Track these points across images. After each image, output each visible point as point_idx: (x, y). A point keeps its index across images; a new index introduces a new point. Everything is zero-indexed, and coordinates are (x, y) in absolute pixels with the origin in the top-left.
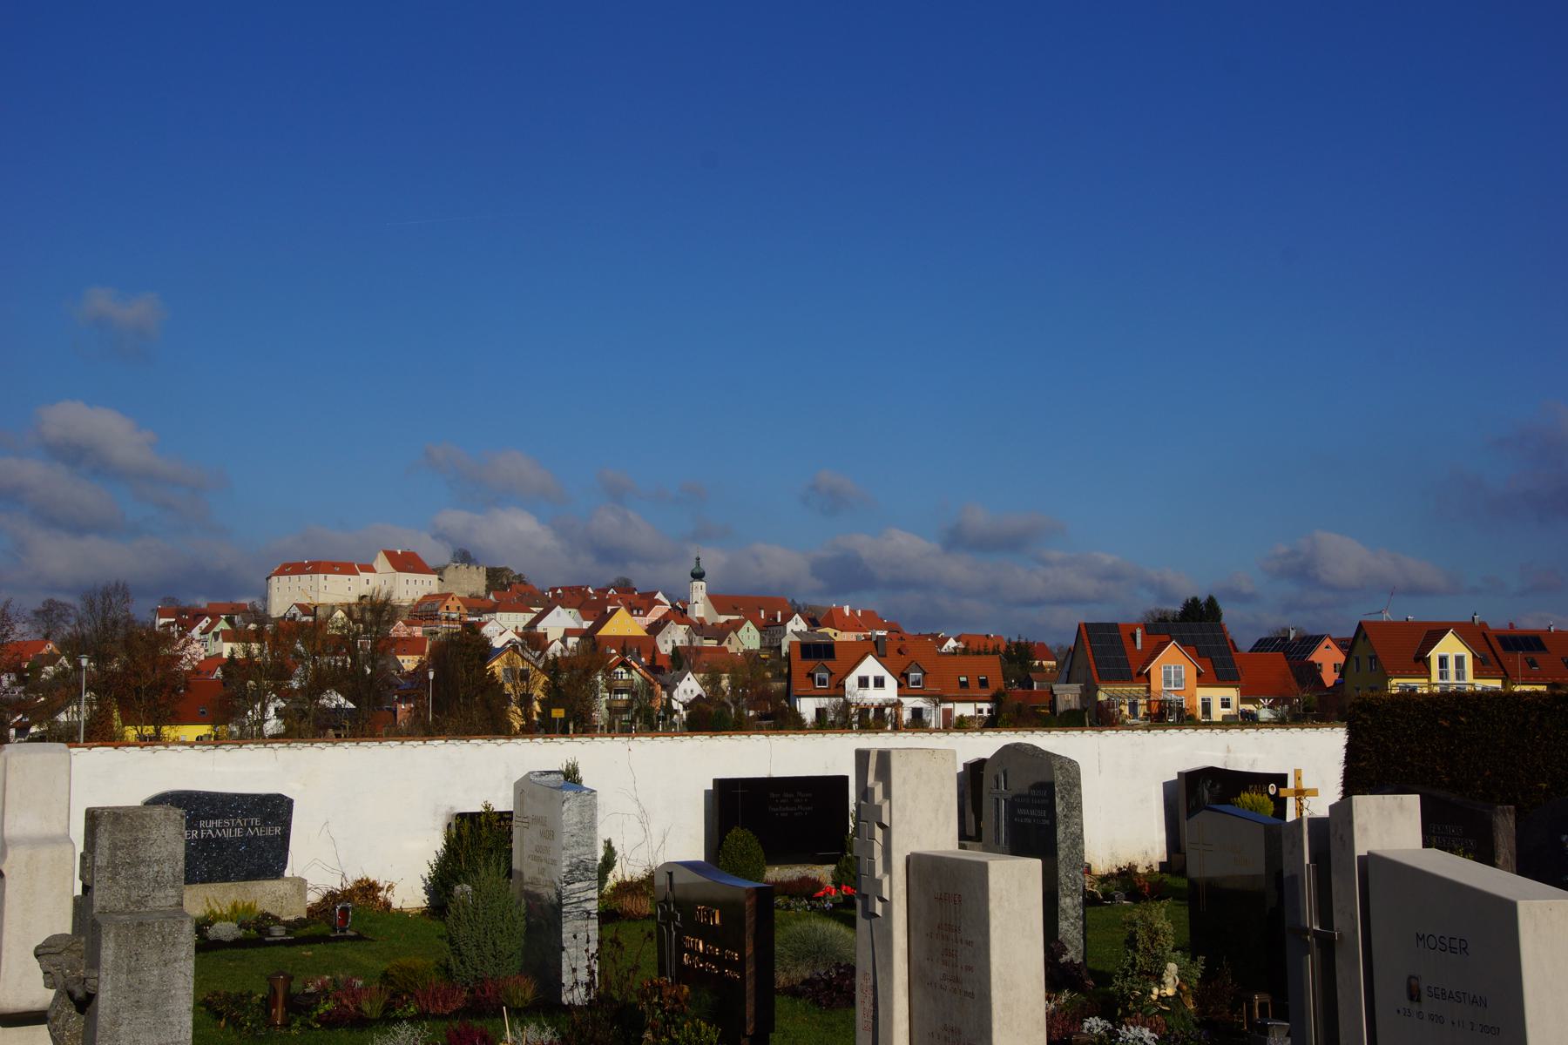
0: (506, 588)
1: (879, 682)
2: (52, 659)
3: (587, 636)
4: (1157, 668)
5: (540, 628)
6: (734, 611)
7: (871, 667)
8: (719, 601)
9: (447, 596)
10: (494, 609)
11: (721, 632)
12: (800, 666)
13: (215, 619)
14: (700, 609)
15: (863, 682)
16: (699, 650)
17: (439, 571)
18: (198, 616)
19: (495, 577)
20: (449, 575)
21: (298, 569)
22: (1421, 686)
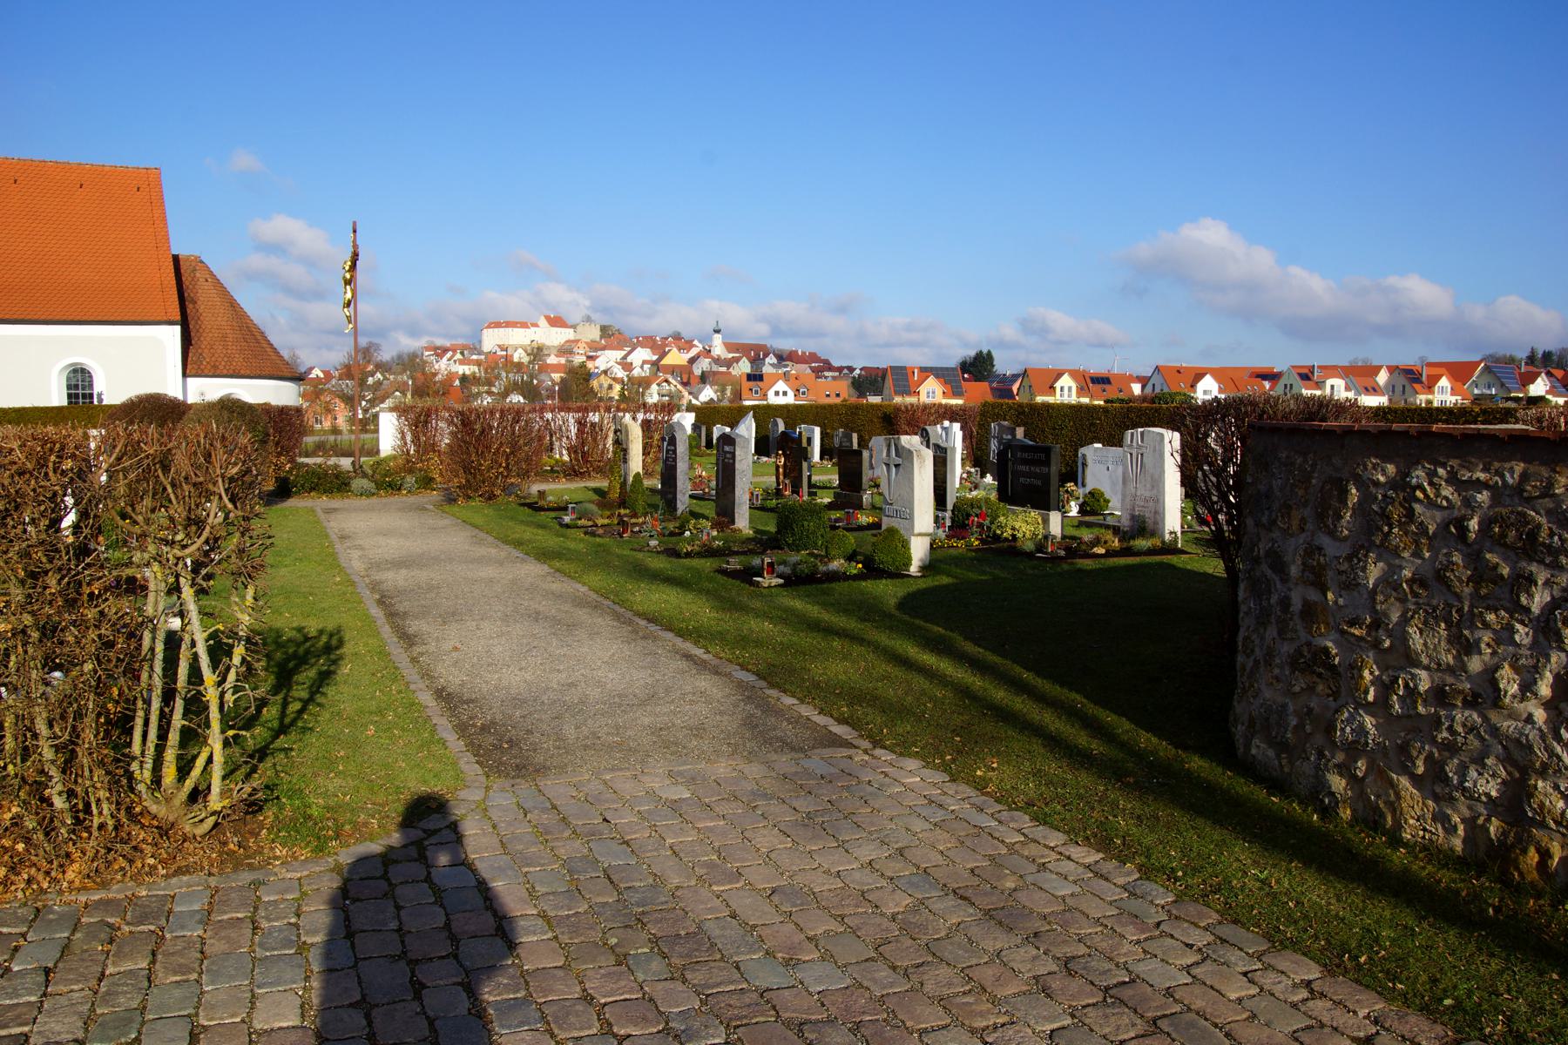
0: (611, 337)
1: (785, 393)
3: (656, 365)
4: (923, 389)
5: (629, 359)
6: (737, 351)
7: (781, 386)
8: (729, 347)
9: (577, 341)
10: (604, 348)
11: (729, 363)
12: (746, 385)
13: (454, 351)
14: (719, 350)
15: (777, 393)
16: (715, 373)
17: (574, 327)
18: (445, 351)
19: (605, 330)
21: (498, 325)
22: (1050, 399)
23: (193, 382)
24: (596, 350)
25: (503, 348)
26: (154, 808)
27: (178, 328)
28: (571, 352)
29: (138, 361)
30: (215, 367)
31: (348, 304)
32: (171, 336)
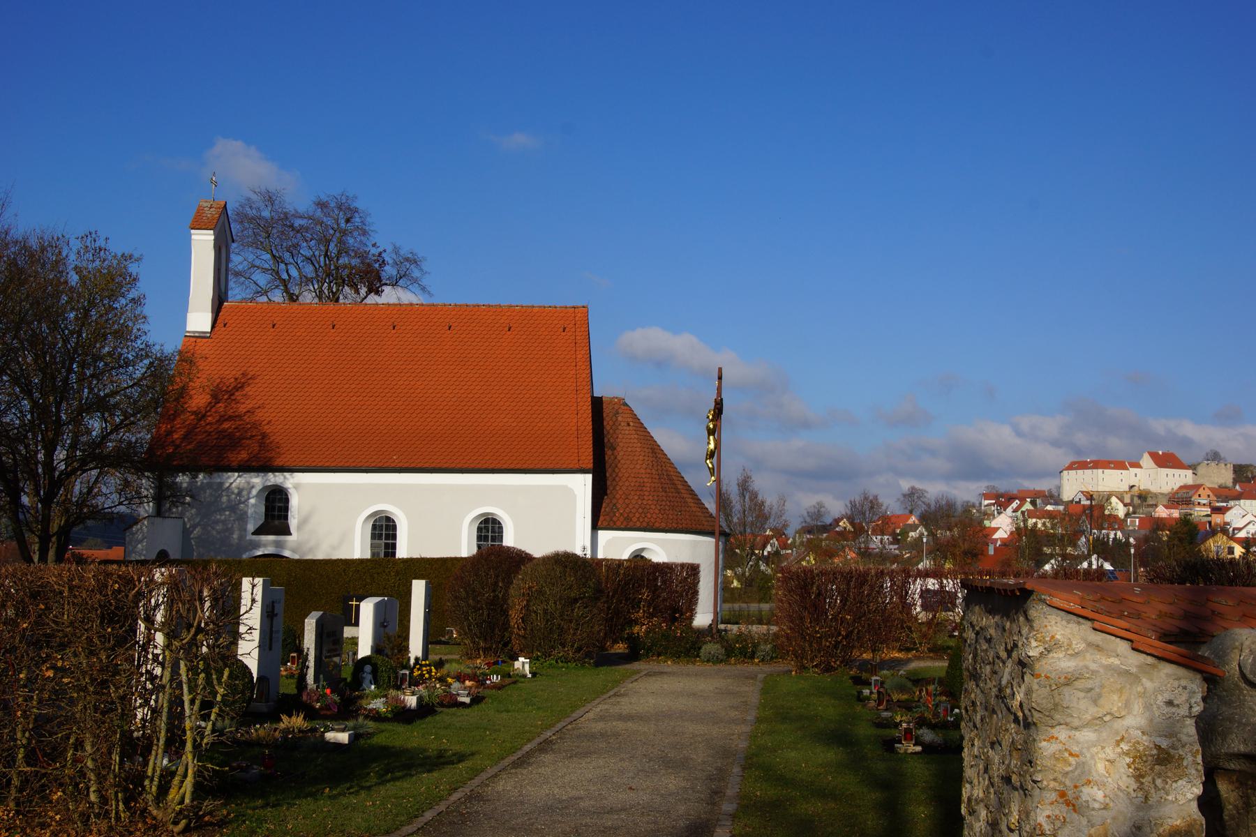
2: (914, 527)
9: (1196, 487)
10: (1239, 497)
13: (1023, 501)
17: (1193, 467)
18: (1011, 499)
19: (1240, 472)
20: (1201, 470)
21: (1083, 465)
23: (603, 535)
24: (1226, 499)
25: (1090, 497)
26: (155, 812)
27: (589, 477)
28: (1188, 502)
29: (550, 514)
30: (628, 519)
31: (711, 455)
32: (582, 484)
